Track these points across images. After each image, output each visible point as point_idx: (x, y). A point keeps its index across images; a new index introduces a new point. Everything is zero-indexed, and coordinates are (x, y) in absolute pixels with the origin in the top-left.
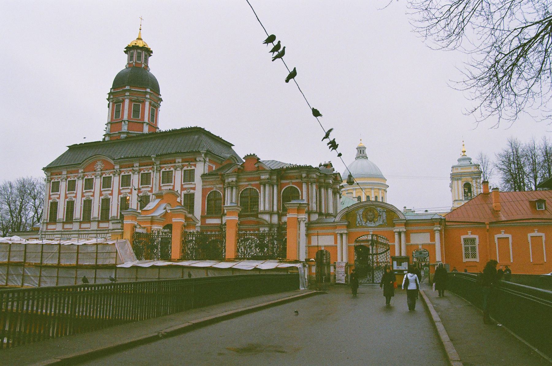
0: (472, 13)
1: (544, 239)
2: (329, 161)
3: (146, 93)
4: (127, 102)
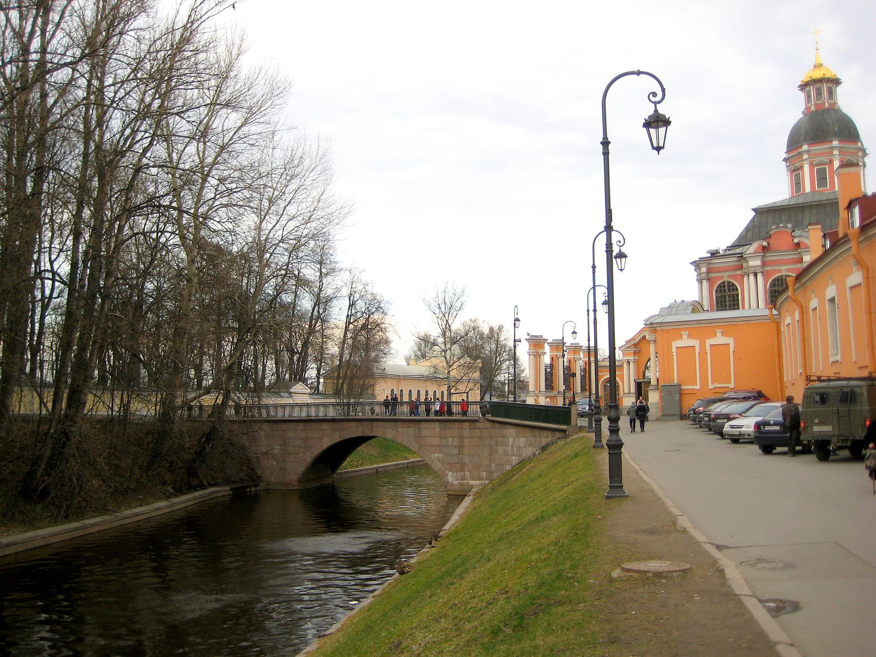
0: (203, 17)
1: (697, 349)
2: (765, 392)
3: (832, 148)
4: (806, 168)
